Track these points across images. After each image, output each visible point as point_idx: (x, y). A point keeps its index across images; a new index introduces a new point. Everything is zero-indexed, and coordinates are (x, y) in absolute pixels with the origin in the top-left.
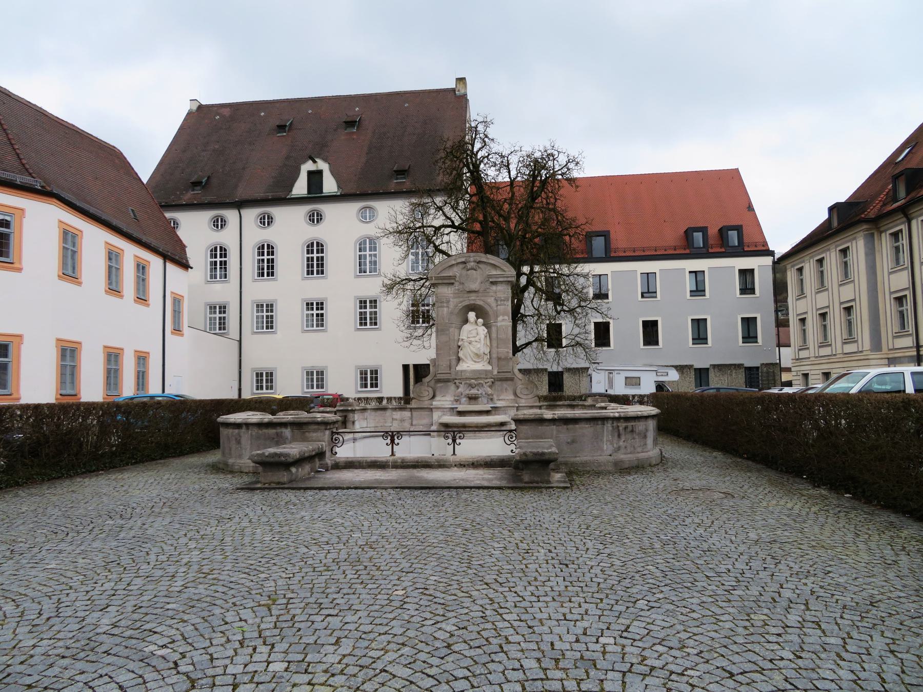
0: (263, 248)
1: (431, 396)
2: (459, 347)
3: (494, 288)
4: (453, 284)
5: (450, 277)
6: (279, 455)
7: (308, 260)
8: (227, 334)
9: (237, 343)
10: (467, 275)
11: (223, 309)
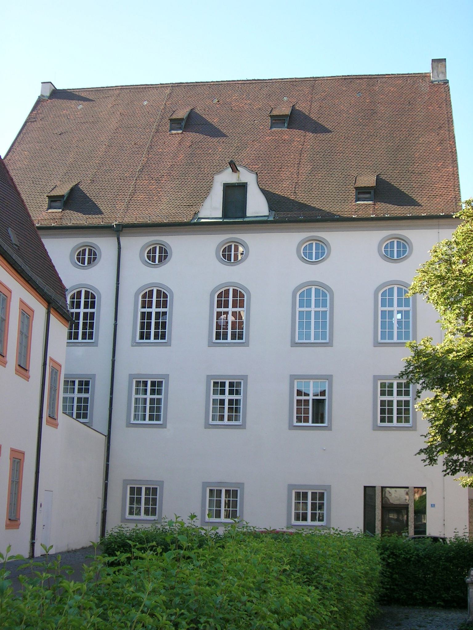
0: (151, 296)
7: (143, 317)
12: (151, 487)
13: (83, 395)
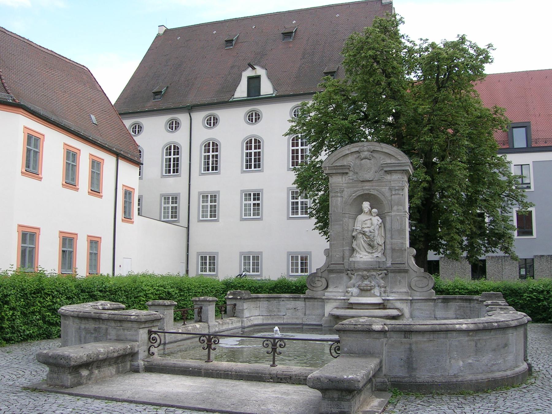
0: (251, 142)
1: (325, 285)
2: (354, 237)
3: (388, 177)
4: (347, 173)
5: (343, 167)
6: (63, 357)
8: (178, 221)
9: (185, 230)
10: (361, 164)
11: (175, 199)
12: (212, 256)
13: (174, 205)
